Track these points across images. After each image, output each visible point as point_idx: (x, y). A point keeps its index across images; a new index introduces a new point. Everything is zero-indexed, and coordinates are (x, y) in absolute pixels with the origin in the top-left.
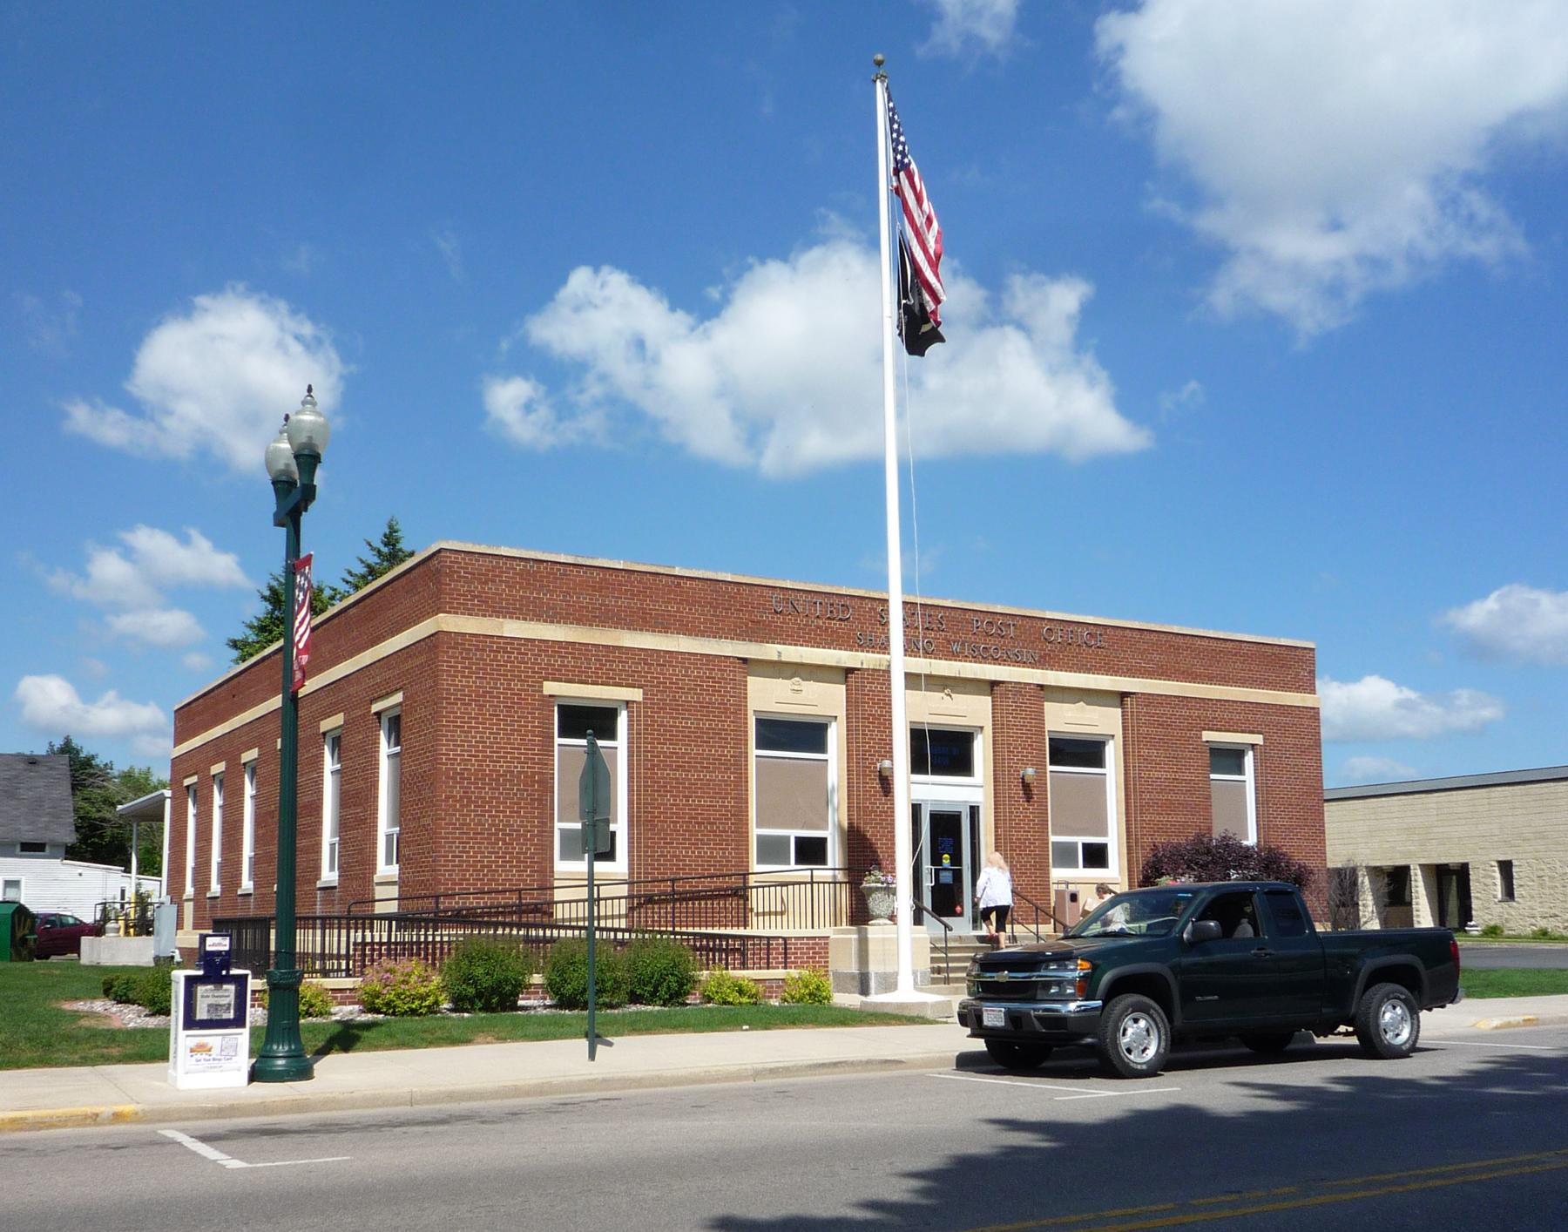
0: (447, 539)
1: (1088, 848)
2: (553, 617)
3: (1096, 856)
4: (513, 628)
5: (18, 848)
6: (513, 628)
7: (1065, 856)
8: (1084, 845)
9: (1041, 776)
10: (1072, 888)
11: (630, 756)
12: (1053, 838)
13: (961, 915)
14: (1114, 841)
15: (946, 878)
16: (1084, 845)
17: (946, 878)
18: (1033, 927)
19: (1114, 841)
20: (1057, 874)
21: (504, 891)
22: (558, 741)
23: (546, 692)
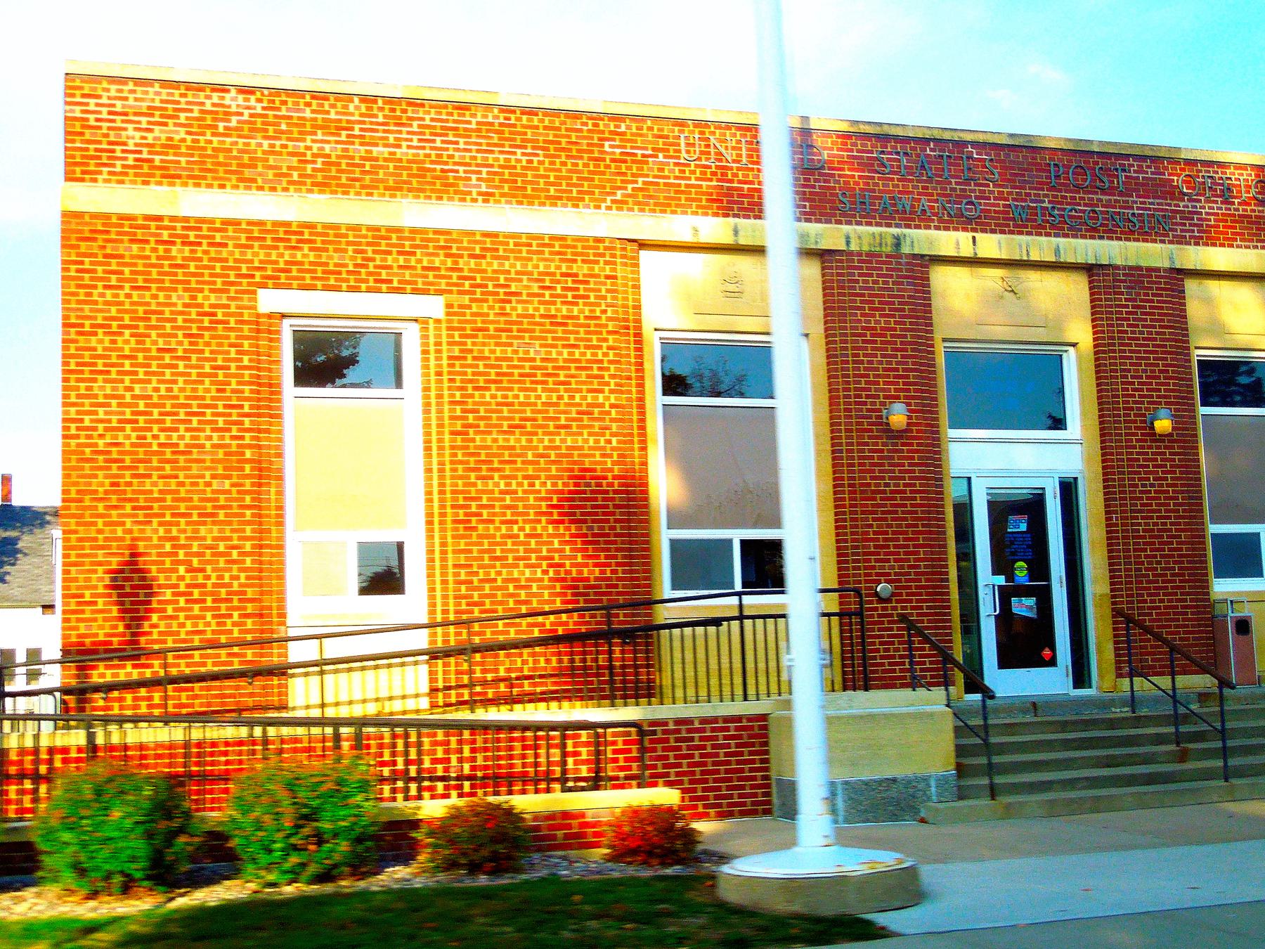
9: (1185, 426)
10: (1244, 611)
13: (1052, 662)
15: (1024, 607)
20: (1222, 587)
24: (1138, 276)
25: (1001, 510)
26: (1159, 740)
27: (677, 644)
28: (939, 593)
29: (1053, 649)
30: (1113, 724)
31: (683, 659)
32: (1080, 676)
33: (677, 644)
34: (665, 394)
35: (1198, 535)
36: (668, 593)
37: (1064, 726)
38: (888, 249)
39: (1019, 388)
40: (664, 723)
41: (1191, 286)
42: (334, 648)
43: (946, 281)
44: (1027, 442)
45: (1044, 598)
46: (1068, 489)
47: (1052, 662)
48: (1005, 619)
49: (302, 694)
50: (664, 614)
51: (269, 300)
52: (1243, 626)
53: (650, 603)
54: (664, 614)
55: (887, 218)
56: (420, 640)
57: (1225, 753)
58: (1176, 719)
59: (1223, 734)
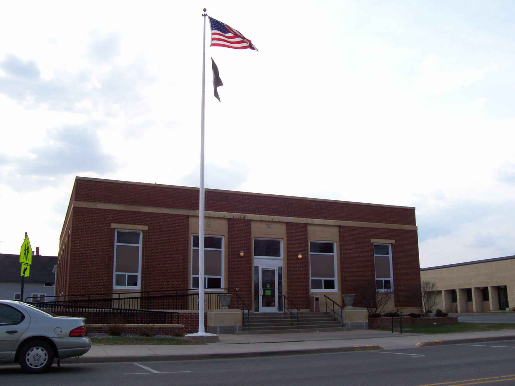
0: (51, 318)
1: (385, 281)
2: (115, 202)
3: (329, 284)
4: (100, 206)
5: (454, 303)
6: (100, 206)
7: (317, 285)
8: (333, 281)
9: (305, 257)
10: (318, 296)
11: (143, 249)
12: (312, 278)
13: (274, 306)
14: (336, 279)
15: (268, 293)
16: (333, 281)
17: (268, 293)
18: (290, 310)
19: (336, 279)
20: (313, 291)
21: (77, 295)
22: (116, 244)
23: (112, 227)
24: (297, 225)
25: (264, 271)
26: (288, 321)
27: (192, 299)
28: (250, 290)
29: (275, 303)
30: (281, 318)
31: (66, 277)
32: (280, 309)
33: (192, 299)
34: (220, 279)
35: (307, 280)
36: (192, 288)
37: (270, 318)
38: (242, 218)
39: (270, 248)
40: (186, 313)
41: (309, 228)
42: (122, 296)
43: (254, 227)
44: (270, 259)
45: (273, 292)
46: (280, 268)
47: (274, 306)
48: (264, 296)
49: (115, 305)
50: (190, 292)
51: (113, 225)
52: (317, 299)
53: (187, 290)
54: (190, 292)
55: (242, 212)
56: (139, 295)
57: (298, 324)
58: (291, 318)
59: (298, 321)
